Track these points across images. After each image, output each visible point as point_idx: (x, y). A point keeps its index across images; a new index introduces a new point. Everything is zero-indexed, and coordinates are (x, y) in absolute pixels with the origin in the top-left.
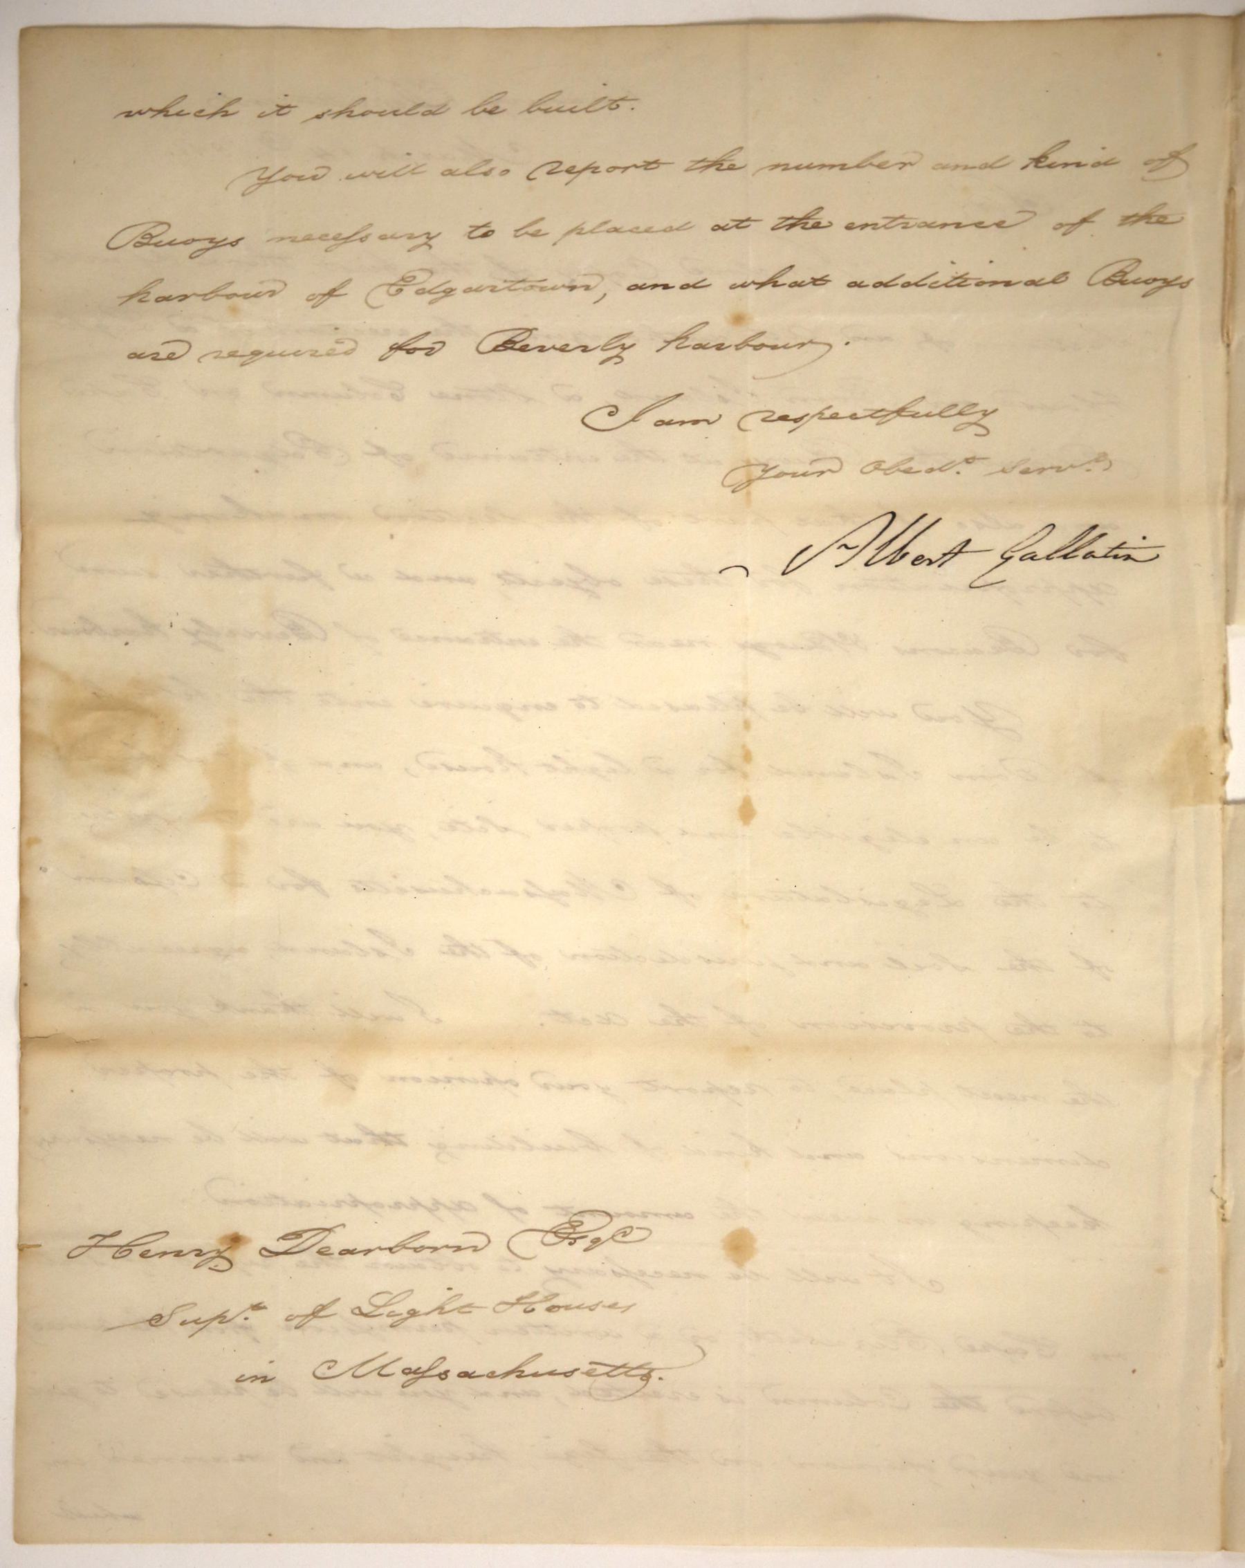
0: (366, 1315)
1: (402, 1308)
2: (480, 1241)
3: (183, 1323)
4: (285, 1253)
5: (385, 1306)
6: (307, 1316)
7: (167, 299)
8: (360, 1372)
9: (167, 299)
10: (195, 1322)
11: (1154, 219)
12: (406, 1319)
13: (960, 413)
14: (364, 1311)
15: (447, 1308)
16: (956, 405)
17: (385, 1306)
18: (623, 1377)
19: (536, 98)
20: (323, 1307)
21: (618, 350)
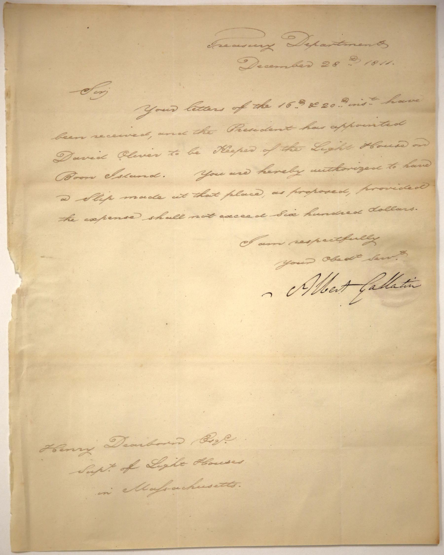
0: (150, 467)
1: (162, 464)
2: (181, 441)
3: (88, 473)
4: (112, 447)
5: (157, 464)
6: (127, 468)
7: (78, 159)
8: (137, 489)
9: (78, 159)
10: (92, 472)
11: (206, 132)
12: (164, 468)
13: (368, 238)
14: (150, 466)
15: (177, 464)
16: (366, 236)
17: (157, 464)
18: (226, 487)
19: (292, 168)
20: (132, 465)
21: (373, 239)
